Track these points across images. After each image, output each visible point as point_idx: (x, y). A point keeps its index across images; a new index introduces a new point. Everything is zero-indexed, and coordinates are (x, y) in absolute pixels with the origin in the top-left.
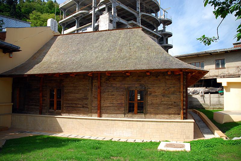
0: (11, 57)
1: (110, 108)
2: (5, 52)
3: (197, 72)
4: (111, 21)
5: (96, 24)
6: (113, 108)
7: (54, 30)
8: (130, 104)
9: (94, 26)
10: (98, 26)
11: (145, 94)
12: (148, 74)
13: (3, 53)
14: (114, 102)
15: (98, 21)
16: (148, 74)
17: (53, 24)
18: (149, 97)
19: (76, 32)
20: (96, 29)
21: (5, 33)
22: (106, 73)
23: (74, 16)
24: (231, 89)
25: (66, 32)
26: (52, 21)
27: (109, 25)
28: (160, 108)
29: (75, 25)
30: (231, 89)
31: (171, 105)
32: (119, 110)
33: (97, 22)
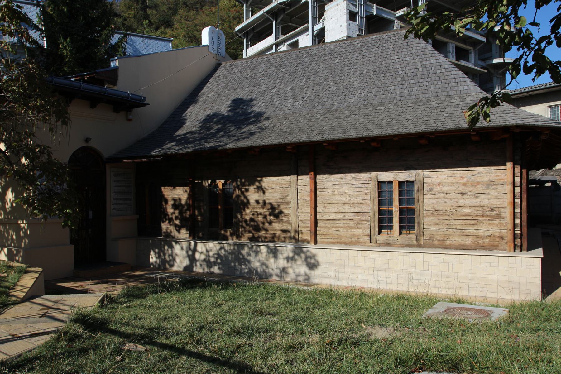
0: (130, 120)
1: (338, 222)
2: (116, 110)
3: (6, 235)
4: (352, 16)
5: (318, 27)
6: (345, 222)
7: (216, 53)
8: (380, 212)
9: (314, 32)
10: (322, 30)
11: (418, 191)
12: (423, 142)
13: (114, 111)
14: (347, 210)
15: (323, 18)
16: (423, 142)
17: (215, 40)
18: (428, 196)
19: (274, 51)
20: (320, 36)
21: (116, 69)
22: (324, 144)
23: (267, 12)
24: (73, 246)
25: (251, 51)
26: (211, 33)
27: (348, 25)
28: (453, 222)
29: (270, 34)
30: (73, 246)
31: (483, 216)
32: (357, 228)
33: (321, 21)
